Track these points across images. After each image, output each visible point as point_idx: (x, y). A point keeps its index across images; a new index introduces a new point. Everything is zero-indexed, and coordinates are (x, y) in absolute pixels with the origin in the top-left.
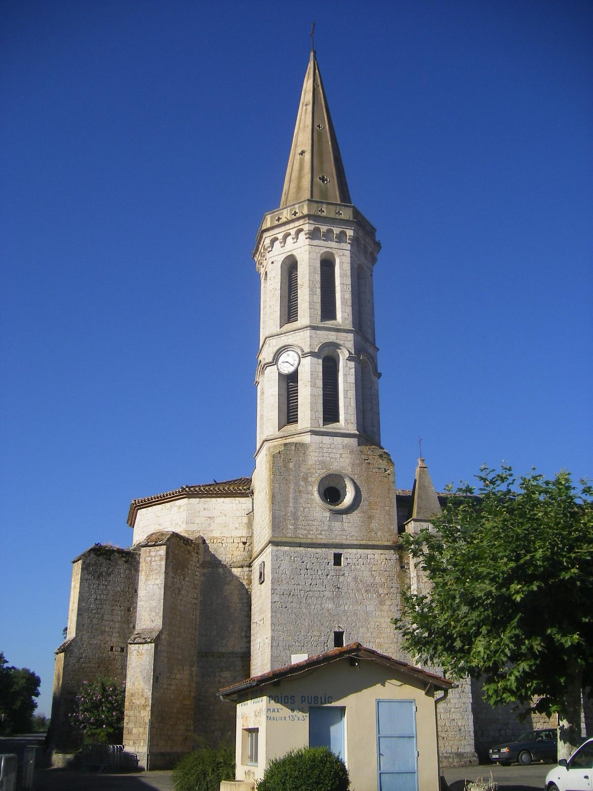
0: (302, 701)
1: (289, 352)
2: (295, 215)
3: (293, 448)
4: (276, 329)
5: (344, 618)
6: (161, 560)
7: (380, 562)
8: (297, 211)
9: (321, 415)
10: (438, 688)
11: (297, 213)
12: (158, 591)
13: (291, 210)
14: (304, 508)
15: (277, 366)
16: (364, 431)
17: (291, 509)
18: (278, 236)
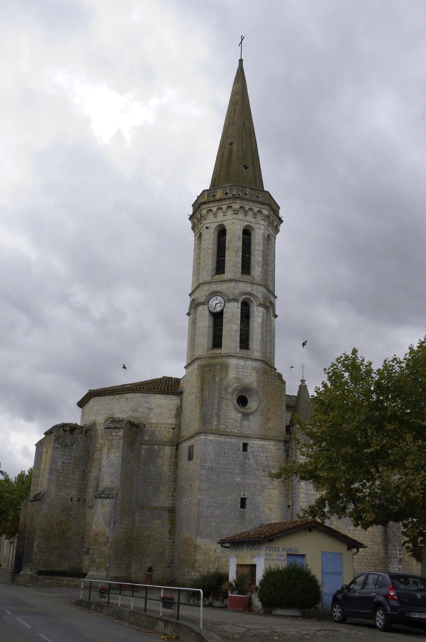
0: (283, 550)
1: (217, 297)
3: (219, 367)
4: (208, 279)
5: (247, 488)
7: (273, 451)
8: (228, 192)
9: (238, 345)
10: (354, 547)
11: (228, 193)
13: (223, 190)
14: (225, 410)
15: (208, 306)
16: (198, 304)
17: (215, 410)
18: (212, 209)
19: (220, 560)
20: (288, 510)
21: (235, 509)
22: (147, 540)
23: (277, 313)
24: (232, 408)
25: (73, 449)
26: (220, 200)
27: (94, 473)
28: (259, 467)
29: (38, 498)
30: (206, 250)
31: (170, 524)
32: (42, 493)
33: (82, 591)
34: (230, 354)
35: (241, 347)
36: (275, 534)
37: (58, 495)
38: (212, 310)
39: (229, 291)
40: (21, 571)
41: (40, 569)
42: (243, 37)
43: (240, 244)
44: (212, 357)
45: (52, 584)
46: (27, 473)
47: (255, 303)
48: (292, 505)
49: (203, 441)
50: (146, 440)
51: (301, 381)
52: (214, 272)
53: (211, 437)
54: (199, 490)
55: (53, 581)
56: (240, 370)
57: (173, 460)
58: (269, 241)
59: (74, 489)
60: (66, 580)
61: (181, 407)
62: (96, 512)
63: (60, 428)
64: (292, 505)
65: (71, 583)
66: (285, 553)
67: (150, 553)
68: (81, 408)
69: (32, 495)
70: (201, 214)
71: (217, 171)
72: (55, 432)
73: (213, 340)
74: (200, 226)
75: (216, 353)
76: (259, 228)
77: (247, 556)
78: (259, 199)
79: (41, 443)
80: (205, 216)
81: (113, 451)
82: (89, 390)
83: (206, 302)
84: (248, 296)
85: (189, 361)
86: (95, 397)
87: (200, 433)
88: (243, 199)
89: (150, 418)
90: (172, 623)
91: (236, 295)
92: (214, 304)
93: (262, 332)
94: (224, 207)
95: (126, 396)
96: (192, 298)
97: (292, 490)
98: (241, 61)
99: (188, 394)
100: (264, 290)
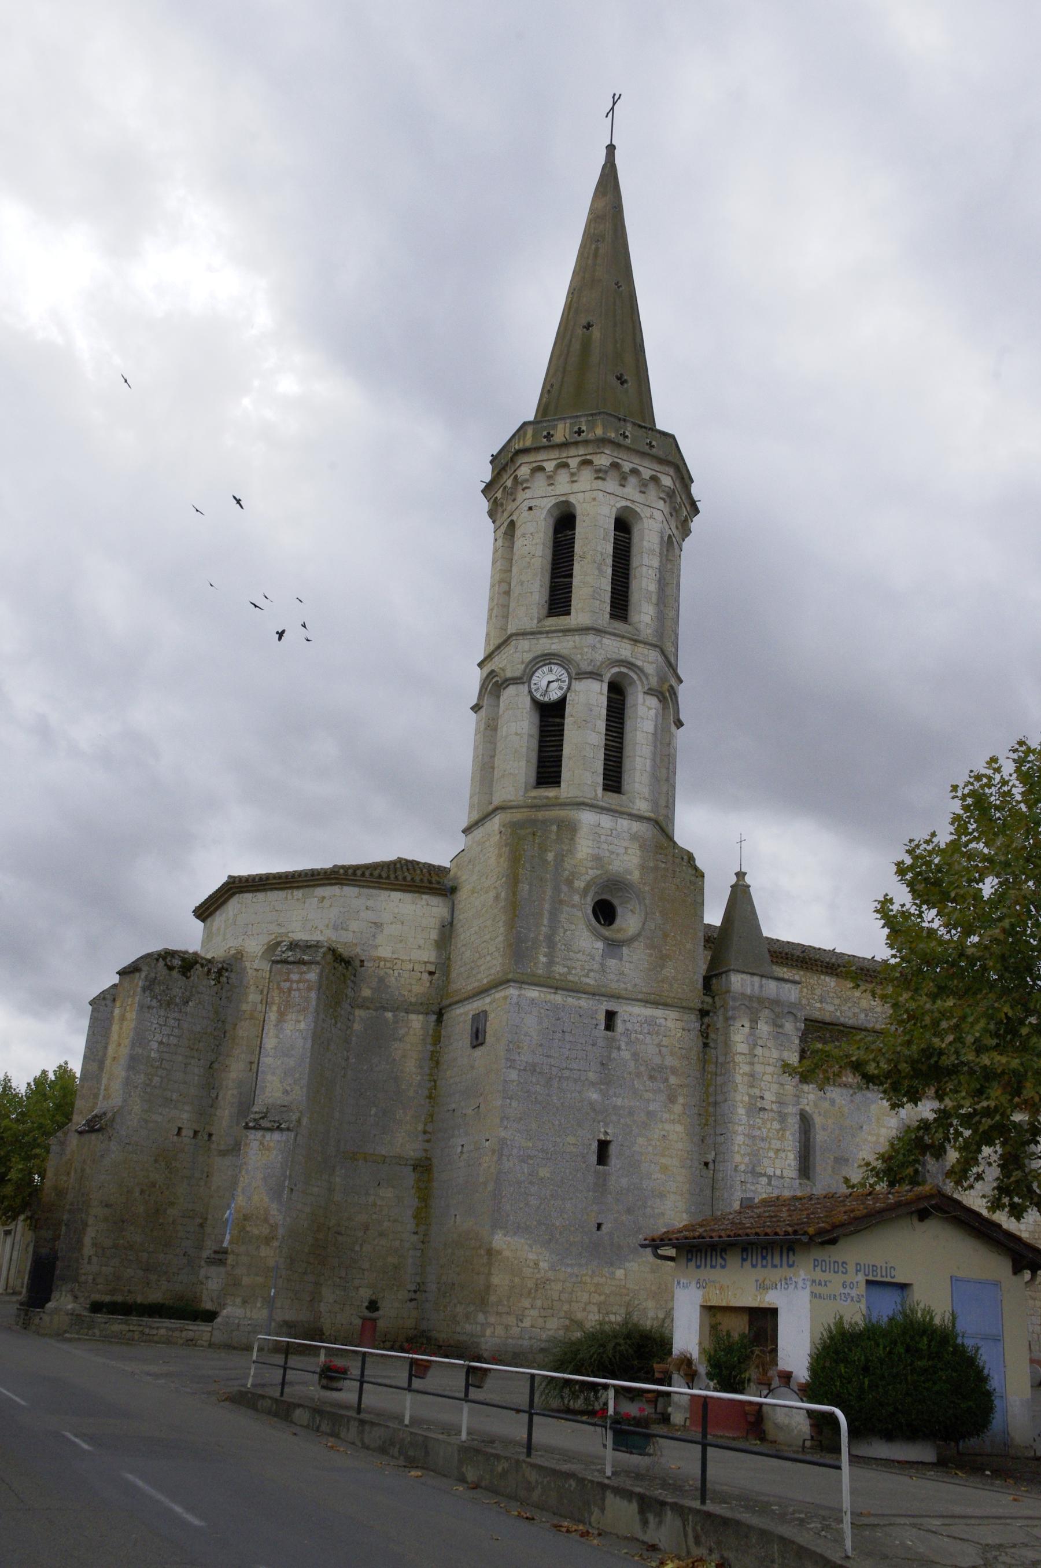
0: (857, 1271)
1: (553, 666)
2: (579, 435)
3: (554, 828)
4: (531, 625)
5: (614, 1118)
6: (309, 989)
7: (673, 1033)
8: (584, 428)
12: (300, 1042)
14: (566, 931)
15: (529, 687)
16: (506, 680)
17: (544, 930)
18: (545, 464)
19: (548, 1287)
20: (704, 1171)
21: (584, 1166)
22: (360, 1234)
23: (682, 717)
24: (582, 926)
25: (186, 1013)
26: (565, 445)
27: (235, 1070)
28: (642, 1069)
29: (95, 1126)
30: (527, 559)
31: (419, 1198)
32: (109, 1115)
33: (253, 1366)
34: (581, 799)
35: (606, 788)
36: (842, 1225)
37: (146, 1121)
38: (538, 696)
39: (581, 654)
40: (48, 1300)
41: (96, 1297)
42: (616, 98)
43: (610, 549)
44: (536, 806)
45: (130, 1334)
46: (51, 1076)
47: (640, 688)
48: (714, 1161)
49: (514, 1000)
50: (365, 999)
51: (737, 874)
52: (545, 611)
53: (533, 993)
54: (502, 1119)
55: (131, 1328)
56: (603, 838)
57: (430, 1048)
58: (671, 547)
59: (187, 1108)
60: (163, 1326)
61: (451, 924)
62: (245, 1163)
63: (157, 960)
64: (714, 1161)
65: (177, 1334)
66: (861, 1278)
67: (366, 1266)
68: (203, 921)
69: (79, 1120)
70: (516, 476)
71: (552, 386)
72: (145, 968)
73: (539, 767)
74: (511, 506)
75: (547, 798)
76: (651, 517)
77: (742, 1286)
78: (654, 450)
79: (104, 999)
80: (527, 481)
81: (291, 1016)
82: (230, 877)
83: (524, 679)
84: (623, 670)
85: (475, 816)
86: (242, 892)
87: (508, 981)
88: (618, 446)
89: (376, 947)
90: (679, 1510)
91: (598, 664)
92: (544, 683)
93: (654, 754)
94: (574, 463)
95: (320, 891)
96: (487, 669)
97: (715, 1127)
98: (611, 149)
99: (473, 892)
100: (660, 659)
